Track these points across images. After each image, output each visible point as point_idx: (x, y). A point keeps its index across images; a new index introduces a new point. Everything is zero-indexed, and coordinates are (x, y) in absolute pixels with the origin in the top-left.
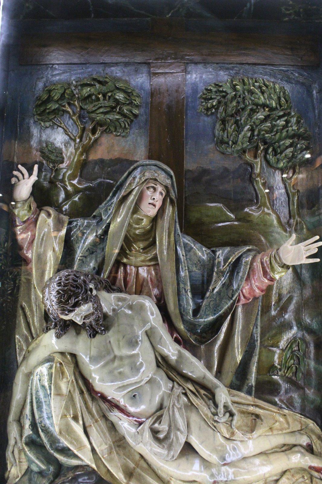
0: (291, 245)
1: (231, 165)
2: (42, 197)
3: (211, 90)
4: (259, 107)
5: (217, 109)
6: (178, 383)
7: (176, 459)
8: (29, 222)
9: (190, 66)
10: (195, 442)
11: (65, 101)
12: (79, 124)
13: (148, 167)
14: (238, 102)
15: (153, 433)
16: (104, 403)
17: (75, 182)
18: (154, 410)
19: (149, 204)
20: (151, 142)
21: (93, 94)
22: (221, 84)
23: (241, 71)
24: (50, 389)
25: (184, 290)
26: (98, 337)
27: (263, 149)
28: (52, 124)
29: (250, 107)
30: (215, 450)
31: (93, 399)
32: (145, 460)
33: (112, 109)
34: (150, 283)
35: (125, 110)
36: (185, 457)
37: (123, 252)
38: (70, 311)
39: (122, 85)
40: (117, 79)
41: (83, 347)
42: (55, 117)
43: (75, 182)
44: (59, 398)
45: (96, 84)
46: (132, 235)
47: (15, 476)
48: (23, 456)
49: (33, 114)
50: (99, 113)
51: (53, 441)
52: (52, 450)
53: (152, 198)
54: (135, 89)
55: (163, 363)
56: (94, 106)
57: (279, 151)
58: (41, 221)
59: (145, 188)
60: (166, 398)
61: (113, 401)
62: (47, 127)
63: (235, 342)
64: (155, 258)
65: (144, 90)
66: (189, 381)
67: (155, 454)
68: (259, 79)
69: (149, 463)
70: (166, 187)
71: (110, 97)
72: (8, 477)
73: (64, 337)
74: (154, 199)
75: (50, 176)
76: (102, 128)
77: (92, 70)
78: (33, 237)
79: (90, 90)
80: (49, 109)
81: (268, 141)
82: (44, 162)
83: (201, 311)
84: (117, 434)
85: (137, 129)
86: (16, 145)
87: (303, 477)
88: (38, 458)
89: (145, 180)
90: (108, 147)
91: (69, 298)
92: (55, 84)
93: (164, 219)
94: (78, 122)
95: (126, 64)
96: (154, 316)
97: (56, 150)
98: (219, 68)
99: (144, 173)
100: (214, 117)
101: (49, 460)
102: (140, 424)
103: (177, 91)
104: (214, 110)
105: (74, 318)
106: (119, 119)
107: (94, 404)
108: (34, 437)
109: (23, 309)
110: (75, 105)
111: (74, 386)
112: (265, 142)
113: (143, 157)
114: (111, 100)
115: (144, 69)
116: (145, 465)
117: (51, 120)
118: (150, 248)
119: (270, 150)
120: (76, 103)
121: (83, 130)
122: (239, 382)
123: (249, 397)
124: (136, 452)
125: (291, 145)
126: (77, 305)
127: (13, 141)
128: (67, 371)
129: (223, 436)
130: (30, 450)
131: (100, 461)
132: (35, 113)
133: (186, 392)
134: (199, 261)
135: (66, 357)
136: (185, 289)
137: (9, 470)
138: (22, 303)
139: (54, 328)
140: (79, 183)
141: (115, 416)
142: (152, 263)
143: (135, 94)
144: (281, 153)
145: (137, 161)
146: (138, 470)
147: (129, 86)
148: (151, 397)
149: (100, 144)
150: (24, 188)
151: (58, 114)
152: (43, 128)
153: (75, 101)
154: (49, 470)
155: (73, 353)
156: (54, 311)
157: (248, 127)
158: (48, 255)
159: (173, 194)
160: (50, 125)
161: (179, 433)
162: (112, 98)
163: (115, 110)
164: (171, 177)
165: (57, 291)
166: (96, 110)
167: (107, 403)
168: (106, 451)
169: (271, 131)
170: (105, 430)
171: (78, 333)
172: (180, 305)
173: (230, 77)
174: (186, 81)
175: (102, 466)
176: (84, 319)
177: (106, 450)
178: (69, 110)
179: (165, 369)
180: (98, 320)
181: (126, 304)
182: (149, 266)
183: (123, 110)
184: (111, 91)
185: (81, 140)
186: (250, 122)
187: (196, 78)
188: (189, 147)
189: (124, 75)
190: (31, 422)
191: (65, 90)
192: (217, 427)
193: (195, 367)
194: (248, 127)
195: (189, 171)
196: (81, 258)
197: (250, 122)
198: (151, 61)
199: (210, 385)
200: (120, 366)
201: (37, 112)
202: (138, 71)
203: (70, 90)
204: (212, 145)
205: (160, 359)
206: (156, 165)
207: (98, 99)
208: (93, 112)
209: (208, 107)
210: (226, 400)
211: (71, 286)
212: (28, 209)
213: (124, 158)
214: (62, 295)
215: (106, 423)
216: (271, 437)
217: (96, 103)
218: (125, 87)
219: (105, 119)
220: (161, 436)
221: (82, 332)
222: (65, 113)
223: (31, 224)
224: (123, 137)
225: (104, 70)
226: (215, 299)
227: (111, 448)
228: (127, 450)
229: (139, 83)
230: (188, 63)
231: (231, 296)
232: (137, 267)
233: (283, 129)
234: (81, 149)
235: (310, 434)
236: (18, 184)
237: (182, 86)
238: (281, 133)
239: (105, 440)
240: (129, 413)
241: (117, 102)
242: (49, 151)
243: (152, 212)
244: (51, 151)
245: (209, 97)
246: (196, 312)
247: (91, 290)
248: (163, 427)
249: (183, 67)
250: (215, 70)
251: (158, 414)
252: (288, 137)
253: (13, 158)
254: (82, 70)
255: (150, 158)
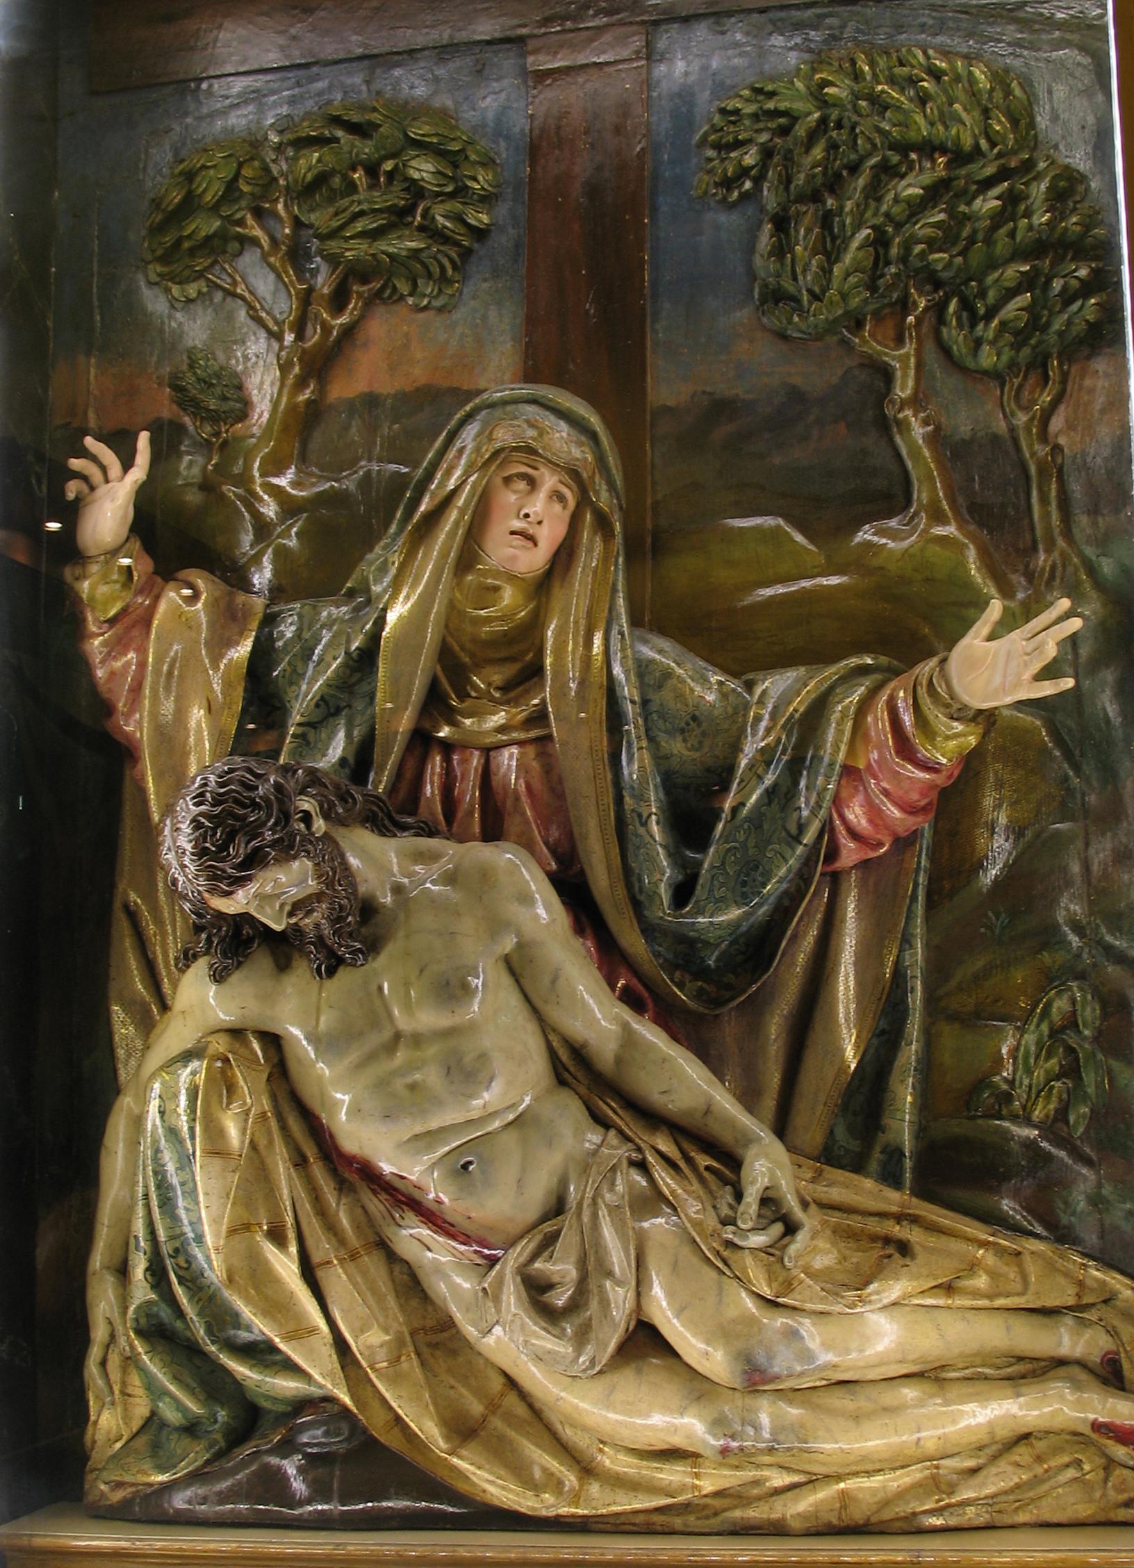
0: (990, 638)
1: (814, 375)
2: (174, 538)
3: (737, 112)
4: (913, 156)
5: (758, 181)
6: (621, 1132)
7: (600, 1372)
8: (127, 621)
9: (667, 32)
10: (663, 1309)
11: (244, 203)
12: (291, 281)
13: (509, 408)
14: (833, 147)
15: (533, 1293)
16: (375, 1193)
17: (282, 482)
18: (532, 1214)
19: (513, 533)
20: (531, 321)
21: (333, 172)
22: (770, 88)
23: (851, 26)
24: (193, 1137)
25: (636, 819)
26: (345, 976)
27: (926, 309)
28: (205, 290)
29: (874, 161)
30: (723, 1333)
31: (343, 1186)
32: (523, 1395)
33: (399, 217)
34: (524, 798)
35: (438, 218)
36: (634, 1365)
37: (436, 703)
38: (240, 882)
39: (427, 129)
40: (407, 111)
41: (298, 1009)
42: (215, 262)
43: (282, 482)
44: (217, 1162)
45: (340, 133)
46: (469, 645)
47: (112, 1436)
48: (135, 1380)
49: (143, 260)
50: (352, 238)
51: (221, 1319)
52: (213, 1343)
53: (522, 513)
54: (477, 138)
55: (574, 1068)
56: (336, 214)
57: (982, 311)
58: (165, 613)
59: (498, 481)
60: (573, 1176)
61: (398, 1184)
62: (190, 301)
63: (835, 999)
64: (539, 717)
65: (508, 138)
66: (664, 1128)
67: (538, 1359)
68: (909, 51)
69: (537, 1405)
70: (574, 474)
71: (390, 175)
72: (94, 1442)
73: (235, 978)
74: (527, 516)
75: (205, 468)
76: (365, 288)
77: (331, 87)
78: (142, 665)
79: (319, 161)
80: (189, 237)
81: (945, 275)
82: (187, 420)
83: (699, 887)
84: (430, 1308)
85: (485, 280)
86: (92, 370)
87: (1078, 1463)
88: (176, 1379)
89: (496, 453)
90: (394, 349)
91: (230, 838)
92: (206, 150)
93: (572, 585)
94: (286, 272)
95: (445, 51)
96: (544, 912)
97: (218, 377)
98: (770, 28)
99: (491, 433)
100: (750, 210)
101: (214, 1384)
102: (493, 1261)
103: (618, 130)
104: (748, 185)
105: (256, 909)
106: (421, 250)
107: (344, 1201)
108: (165, 1313)
109: (133, 916)
110: (275, 215)
111: (270, 1133)
112: (933, 281)
113: (507, 376)
114: (397, 186)
115: (506, 61)
116: (521, 1410)
117: (200, 275)
118: (527, 685)
119: (953, 306)
120: (280, 207)
121: (306, 298)
122: (854, 1137)
123: (894, 1195)
124: (493, 1365)
125: (1028, 283)
126: (255, 861)
127: (82, 358)
128: (242, 1083)
129: (754, 1292)
130: (151, 1351)
131: (369, 1388)
132: (149, 257)
133: (644, 1159)
134: (694, 718)
135: (247, 1045)
136: (640, 816)
137: (93, 1418)
138: (128, 895)
139: (207, 953)
140: (295, 484)
141: (412, 1237)
142: (533, 734)
143: (473, 157)
144: (989, 317)
145: (479, 392)
146: (497, 1423)
147: (456, 128)
148: (523, 1170)
149: (365, 345)
150: (109, 512)
151: (225, 252)
152: (177, 305)
153: (277, 200)
154: (216, 1421)
155: (267, 1029)
156: (189, 887)
157: (866, 232)
158: (193, 724)
159: (604, 495)
160: (200, 293)
161: (608, 1284)
162: (398, 177)
163: (410, 219)
164: (593, 436)
165: (193, 821)
166: (342, 227)
167: (383, 1196)
168: (382, 1354)
169: (947, 237)
170: (384, 1285)
171: (283, 966)
172: (627, 871)
173: (806, 56)
174: (649, 88)
175: (375, 1404)
176: (291, 915)
177: (384, 1350)
178: (258, 232)
179: (583, 1090)
180: (340, 919)
181: (437, 869)
182: (520, 743)
183: (434, 218)
184: (393, 156)
185: (300, 336)
186: (875, 215)
187: (686, 74)
188: (663, 328)
189: (435, 93)
190: (149, 1261)
191: (241, 165)
192: (730, 1262)
193: (683, 1078)
194: (866, 232)
195: (666, 410)
196: (300, 730)
197: (875, 215)
198: (524, 31)
199: (727, 1137)
200: (411, 1067)
201: (153, 251)
202: (486, 72)
203: (256, 163)
204: (745, 311)
205: (564, 1055)
206: (533, 401)
207: (352, 187)
208: (333, 234)
209: (726, 174)
210: (772, 1176)
211: (236, 801)
212: (123, 579)
213: (445, 384)
214: (206, 832)
215: (391, 1272)
216: (942, 1316)
217: (345, 202)
218: (437, 135)
219: (373, 255)
220: (560, 1299)
221: (294, 963)
222: (246, 247)
223: (133, 626)
224: (440, 310)
225: (368, 82)
226: (744, 846)
227: (399, 1342)
228: (460, 1359)
229: (490, 115)
230: (656, 23)
231: (794, 831)
232: (488, 751)
233: (994, 228)
234: (297, 369)
235: (1116, 1322)
236: (89, 499)
237: (638, 109)
238: (989, 241)
239: (381, 1319)
240: (452, 1225)
241: (416, 191)
242: (199, 380)
243: (533, 560)
244: (205, 382)
245: (731, 138)
246: (683, 893)
247: (307, 818)
248: (561, 1268)
249: (638, 42)
250: (755, 36)
251: (548, 1227)
252: (1018, 255)
253: (86, 413)
254: (297, 91)
255: (530, 375)
